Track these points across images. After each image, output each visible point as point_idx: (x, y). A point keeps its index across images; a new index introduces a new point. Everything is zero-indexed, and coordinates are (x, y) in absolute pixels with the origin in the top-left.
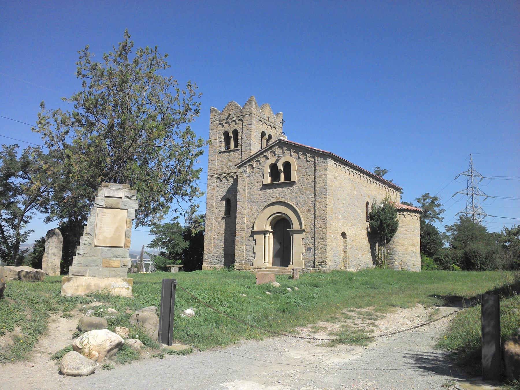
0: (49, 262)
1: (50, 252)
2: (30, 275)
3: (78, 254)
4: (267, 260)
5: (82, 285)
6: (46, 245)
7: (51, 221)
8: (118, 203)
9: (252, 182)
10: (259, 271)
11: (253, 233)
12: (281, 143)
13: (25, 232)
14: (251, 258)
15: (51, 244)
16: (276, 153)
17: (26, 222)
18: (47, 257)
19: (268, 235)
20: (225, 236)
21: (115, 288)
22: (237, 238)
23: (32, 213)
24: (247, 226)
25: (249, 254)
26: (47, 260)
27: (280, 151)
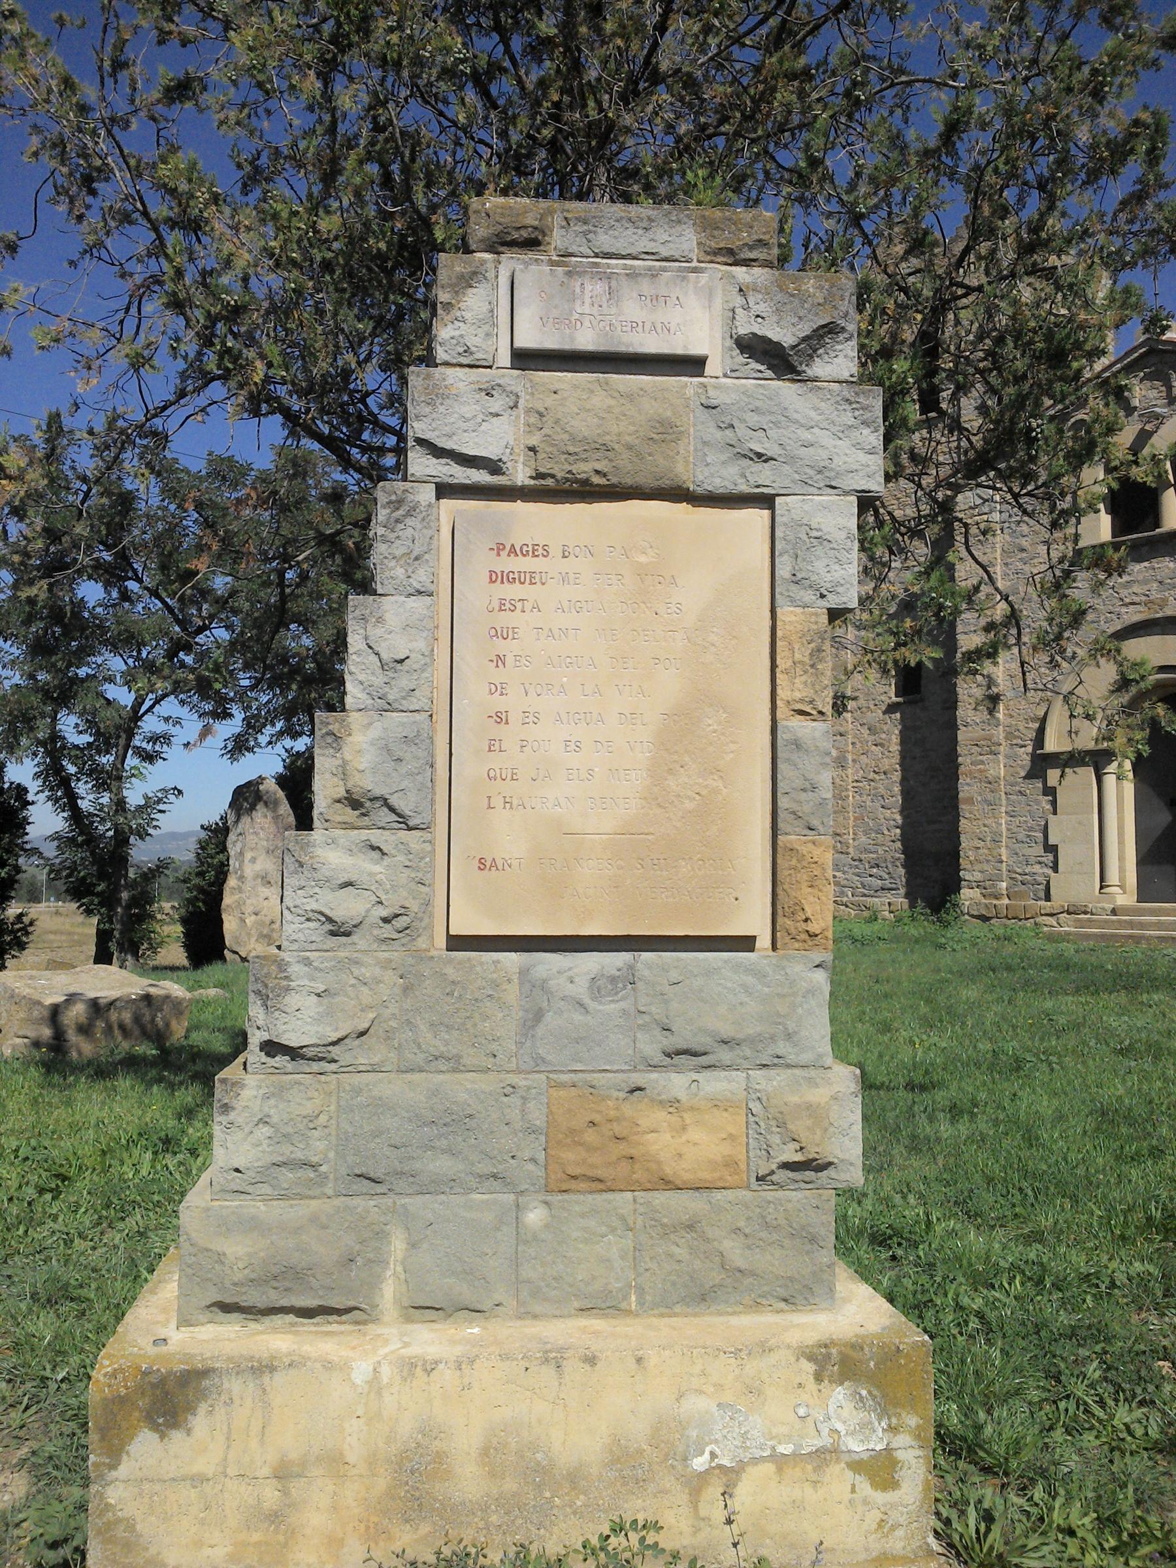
0: (249, 909)
1: (249, 870)
2: (114, 1016)
3: (271, 1048)
4: (1113, 877)
5: (335, 1462)
6: (234, 845)
7: (250, 750)
8: (666, 432)
9: (1024, 543)
10: (1081, 924)
11: (1041, 763)
12: (1153, 359)
13: (146, 797)
14: (1037, 868)
15: (251, 839)
16: (1136, 402)
17: (149, 758)
18: (240, 890)
19: (1112, 767)
20: (904, 781)
21: (730, 1476)
22: (967, 788)
23: (167, 719)
24: (1009, 736)
25: (1028, 851)
26: (240, 904)
27: (1153, 394)
